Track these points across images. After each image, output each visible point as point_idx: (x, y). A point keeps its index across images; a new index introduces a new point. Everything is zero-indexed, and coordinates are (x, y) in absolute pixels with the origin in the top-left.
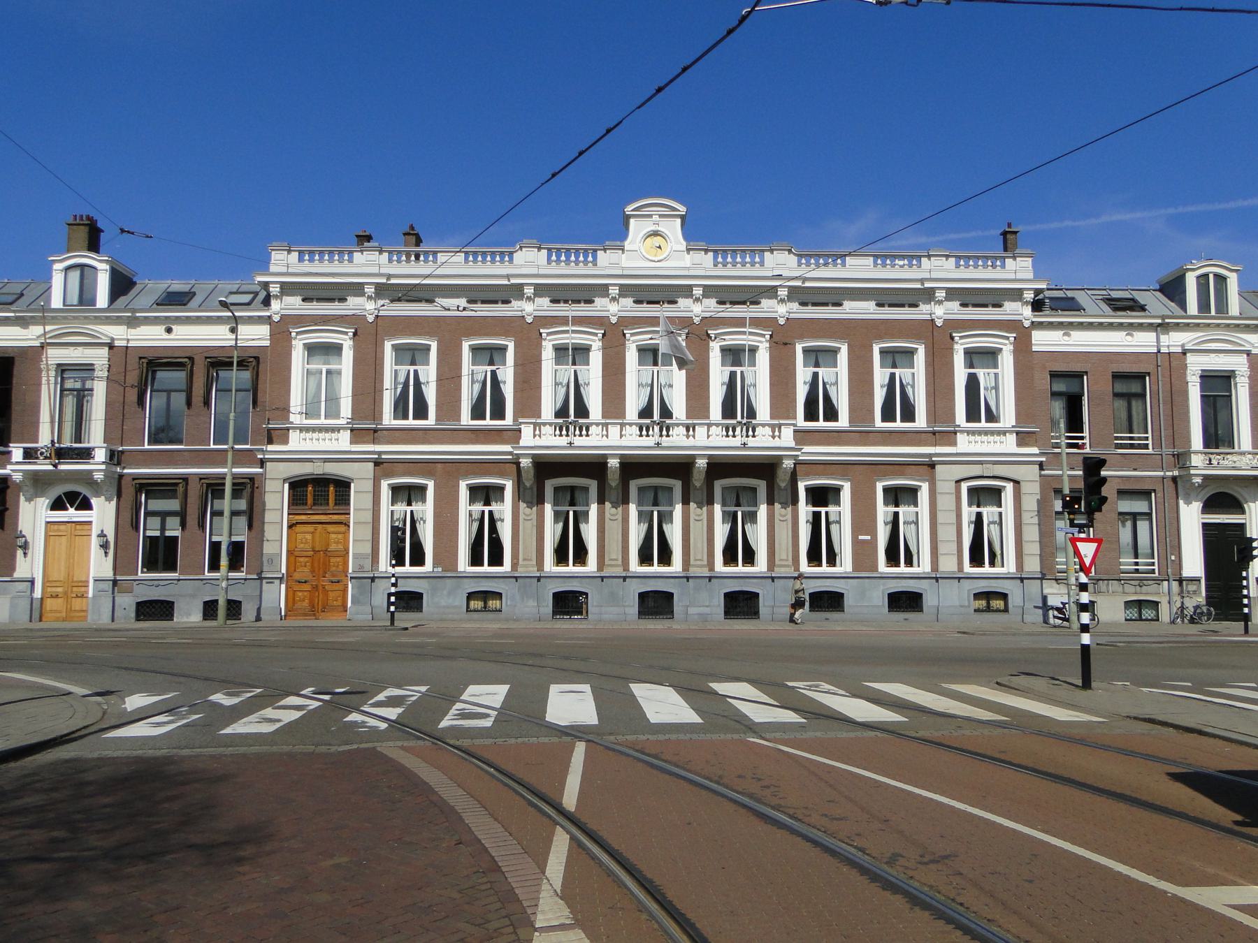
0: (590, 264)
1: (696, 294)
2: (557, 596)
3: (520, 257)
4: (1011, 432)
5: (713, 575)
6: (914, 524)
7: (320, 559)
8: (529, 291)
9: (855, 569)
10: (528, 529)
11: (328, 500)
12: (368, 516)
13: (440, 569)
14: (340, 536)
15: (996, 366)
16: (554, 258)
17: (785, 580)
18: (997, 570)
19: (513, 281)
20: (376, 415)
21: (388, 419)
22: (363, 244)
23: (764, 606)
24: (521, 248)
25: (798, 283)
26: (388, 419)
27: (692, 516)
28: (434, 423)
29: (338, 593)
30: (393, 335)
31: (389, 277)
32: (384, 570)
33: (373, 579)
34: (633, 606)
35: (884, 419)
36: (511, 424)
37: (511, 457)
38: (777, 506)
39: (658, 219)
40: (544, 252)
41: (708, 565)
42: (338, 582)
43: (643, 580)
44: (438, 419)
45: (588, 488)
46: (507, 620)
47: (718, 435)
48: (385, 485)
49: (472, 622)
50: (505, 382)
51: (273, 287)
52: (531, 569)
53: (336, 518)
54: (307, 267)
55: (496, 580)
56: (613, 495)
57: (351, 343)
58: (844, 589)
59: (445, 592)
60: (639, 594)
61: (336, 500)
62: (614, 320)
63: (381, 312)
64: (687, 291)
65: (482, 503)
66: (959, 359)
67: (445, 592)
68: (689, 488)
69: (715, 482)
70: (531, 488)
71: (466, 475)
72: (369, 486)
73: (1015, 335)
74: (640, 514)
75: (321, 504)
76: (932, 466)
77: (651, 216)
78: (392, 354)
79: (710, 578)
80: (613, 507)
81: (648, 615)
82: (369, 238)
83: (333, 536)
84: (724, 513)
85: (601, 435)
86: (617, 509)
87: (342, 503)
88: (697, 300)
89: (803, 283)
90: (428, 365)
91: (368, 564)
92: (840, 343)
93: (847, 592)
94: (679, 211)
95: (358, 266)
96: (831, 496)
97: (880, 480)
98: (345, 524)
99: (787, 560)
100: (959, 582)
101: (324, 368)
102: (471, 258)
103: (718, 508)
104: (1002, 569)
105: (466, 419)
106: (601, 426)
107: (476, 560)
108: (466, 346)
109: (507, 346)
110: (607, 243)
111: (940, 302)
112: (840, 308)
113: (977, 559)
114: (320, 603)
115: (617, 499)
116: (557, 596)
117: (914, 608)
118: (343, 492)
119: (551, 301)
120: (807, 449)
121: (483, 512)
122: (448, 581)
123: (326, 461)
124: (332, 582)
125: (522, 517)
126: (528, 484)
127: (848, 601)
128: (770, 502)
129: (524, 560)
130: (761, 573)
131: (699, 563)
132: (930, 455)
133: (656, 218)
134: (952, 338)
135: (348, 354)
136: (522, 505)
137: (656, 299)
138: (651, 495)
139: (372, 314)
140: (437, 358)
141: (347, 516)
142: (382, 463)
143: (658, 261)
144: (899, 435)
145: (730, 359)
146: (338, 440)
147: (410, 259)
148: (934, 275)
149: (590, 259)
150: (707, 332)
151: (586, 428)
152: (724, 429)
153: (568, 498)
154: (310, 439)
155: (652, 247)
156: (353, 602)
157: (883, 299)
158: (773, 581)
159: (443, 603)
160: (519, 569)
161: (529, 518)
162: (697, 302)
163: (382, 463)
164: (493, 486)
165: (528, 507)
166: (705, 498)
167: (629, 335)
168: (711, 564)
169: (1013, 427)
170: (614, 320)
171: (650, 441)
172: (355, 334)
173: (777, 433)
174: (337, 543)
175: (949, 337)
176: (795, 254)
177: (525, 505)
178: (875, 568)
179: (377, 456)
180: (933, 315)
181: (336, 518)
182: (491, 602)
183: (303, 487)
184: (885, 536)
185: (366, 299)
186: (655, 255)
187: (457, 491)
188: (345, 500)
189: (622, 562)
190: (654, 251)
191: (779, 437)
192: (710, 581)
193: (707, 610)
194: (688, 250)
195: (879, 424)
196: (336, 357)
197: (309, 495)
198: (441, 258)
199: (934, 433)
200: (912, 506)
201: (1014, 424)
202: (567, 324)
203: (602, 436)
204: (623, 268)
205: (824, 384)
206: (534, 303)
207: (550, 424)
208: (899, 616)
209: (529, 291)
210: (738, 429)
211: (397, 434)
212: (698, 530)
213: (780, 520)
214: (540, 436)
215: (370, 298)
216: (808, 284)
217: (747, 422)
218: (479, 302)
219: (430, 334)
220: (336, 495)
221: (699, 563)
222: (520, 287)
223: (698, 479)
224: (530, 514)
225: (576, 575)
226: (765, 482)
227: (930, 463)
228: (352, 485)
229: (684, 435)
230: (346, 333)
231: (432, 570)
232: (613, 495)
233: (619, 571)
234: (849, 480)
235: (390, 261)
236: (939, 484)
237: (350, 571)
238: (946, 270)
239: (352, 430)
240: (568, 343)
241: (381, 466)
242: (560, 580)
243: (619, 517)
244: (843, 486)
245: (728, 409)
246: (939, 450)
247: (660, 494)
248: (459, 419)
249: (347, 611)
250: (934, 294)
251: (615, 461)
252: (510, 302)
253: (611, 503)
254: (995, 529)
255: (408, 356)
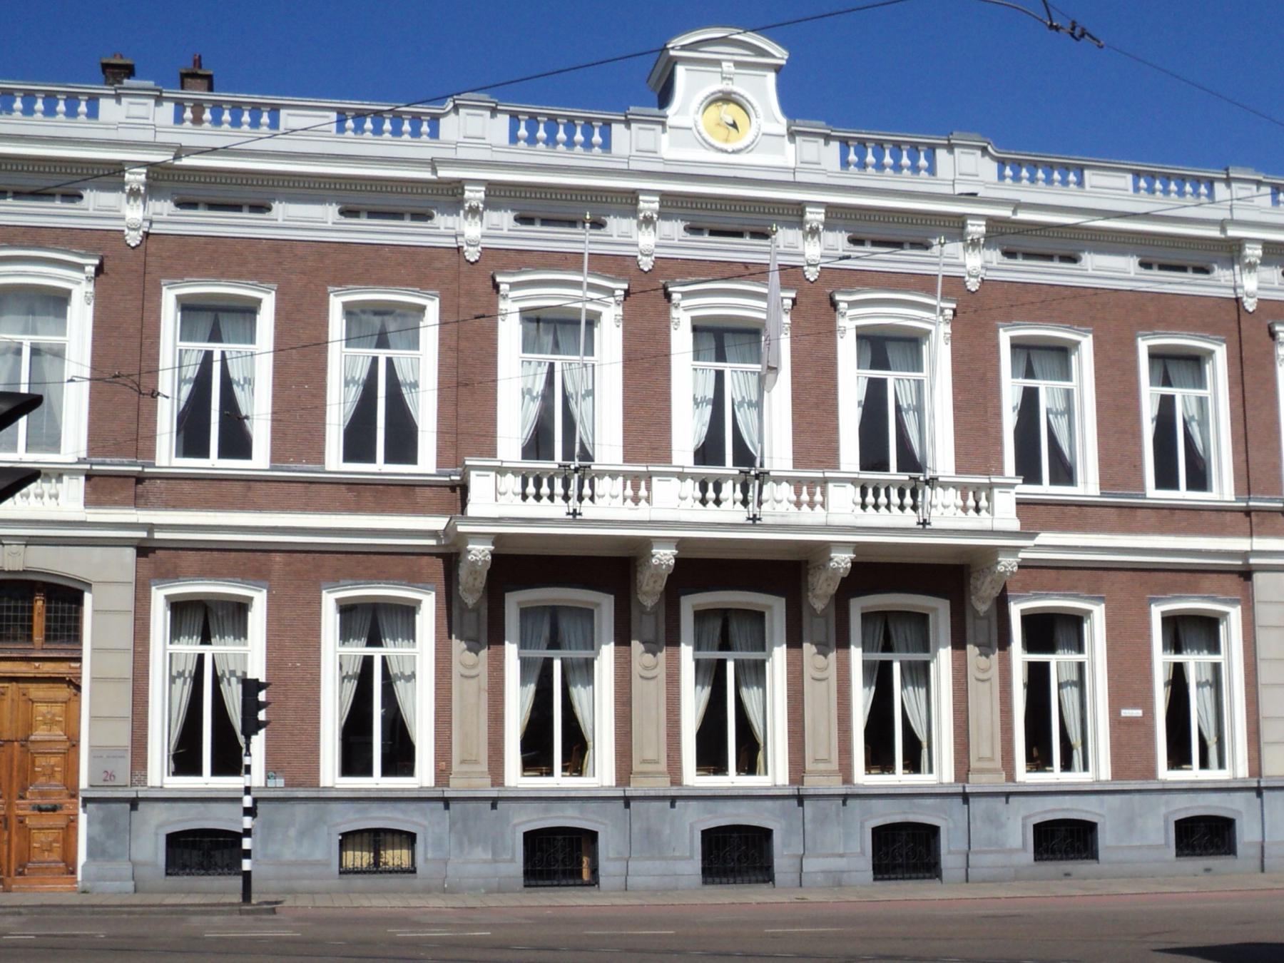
0: (597, 150)
1: (813, 220)
2: (535, 841)
3: (452, 126)
4: (73, 473)
5: (849, 792)
6: (1208, 687)
7: (12, 760)
8: (474, 195)
9: (1116, 774)
10: (469, 695)
11: (30, 628)
12: (125, 665)
13: (280, 782)
14: (57, 709)
15: (918, 367)
16: (523, 132)
17: (990, 799)
18: (1076, 777)
19: (444, 173)
20: (142, 442)
21: (166, 456)
22: (121, 83)
23: (950, 852)
24: (456, 108)
25: (1005, 212)
26: (166, 456)
27: (808, 672)
28: (267, 466)
29: (51, 836)
30: (179, 274)
31: (180, 151)
32: (158, 784)
33: (134, 803)
34: (691, 857)
35: (350, 455)
36: (433, 471)
37: (433, 542)
38: (972, 650)
39: (733, 69)
40: (504, 120)
41: (840, 770)
42: (54, 809)
43: (710, 804)
44: (277, 456)
45: (592, 611)
46: (428, 890)
47: (614, 497)
48: (159, 598)
49: (191, 895)
50: (415, 385)
51: (470, 191)
52: (477, 782)
53: (48, 668)
54: (352, 144)
55: (402, 805)
56: (647, 625)
57: (90, 288)
58: (1096, 814)
59: (292, 832)
60: (705, 833)
61: (48, 628)
62: (646, 263)
63: (154, 226)
64: (793, 214)
65: (364, 641)
66: (847, 348)
67: (292, 832)
68: (801, 613)
69: (507, 595)
70: (476, 609)
71: (336, 580)
72: (125, 598)
73: (954, 306)
74: (525, 664)
75: (15, 639)
76: (1246, 574)
77: (717, 63)
78: (176, 316)
79: (845, 798)
80: (647, 651)
81: (887, 872)
82: (129, 71)
83: (42, 708)
84: (698, 663)
85: (621, 498)
86: (655, 655)
87: (62, 637)
88: (648, 221)
89: (1014, 212)
90: (418, 349)
91: (123, 769)
92: (1079, 332)
93: (602, 826)
94: (773, 56)
95: (108, 126)
96: (1060, 634)
97: (1157, 601)
98: (70, 682)
99: (991, 759)
100: (1007, 802)
101: (27, 341)
102: (350, 124)
103: (511, 651)
104: (1222, 772)
105: (334, 460)
106: (620, 479)
107: (354, 761)
108: (336, 304)
109: (259, 301)
110: (632, 109)
111: (1251, 267)
112: (266, 215)
113: (879, 758)
114: (13, 856)
115: (827, 637)
116: (535, 841)
117: (1079, 851)
118: (63, 611)
119: (342, 213)
120: (1045, 538)
121: (201, 658)
122: (300, 809)
123: (30, 541)
124: (40, 810)
125: (457, 669)
126: (470, 600)
127: (1105, 839)
128: (794, 641)
129: (463, 762)
130: (602, 788)
131: (821, 766)
132: (1245, 555)
133: (728, 67)
134: (834, 305)
135: (429, 334)
136: (458, 646)
137: (1049, 252)
138: (715, 627)
139: (815, 265)
140: (276, 327)
141: (73, 665)
142: (153, 550)
143: (734, 152)
144: (1184, 514)
145: (709, 343)
146: (56, 497)
147: (11, 107)
148: (463, 154)
149: (597, 138)
150: (494, 280)
151: (874, 490)
152: (738, 487)
153: (546, 631)
154: (36, 496)
155: (719, 124)
156: (90, 854)
157: (354, 200)
158: (627, 805)
159: (288, 854)
160: (453, 782)
161: (473, 672)
162: (813, 238)
163: (153, 550)
164: (385, 605)
165: (470, 649)
166: (485, 627)
167: (507, 287)
168: (846, 771)
169: (80, 461)
170: (646, 263)
171: (545, 509)
172: (99, 270)
173: (643, 492)
174: (51, 723)
175: (1268, 334)
176: (993, 158)
177: (463, 645)
178: (1151, 772)
179: (144, 534)
180: (1239, 291)
181: (48, 668)
182: (390, 852)
183: (24, 598)
184: (697, 709)
185: (124, 196)
186: (727, 140)
187: (317, 614)
188: (69, 629)
189: (669, 765)
190: (722, 132)
191: (648, 500)
192: (494, 807)
193: (841, 863)
194: (792, 135)
195: (1154, 494)
196: (51, 319)
197: (36, 618)
198: (288, 119)
199: (1248, 512)
200: (1205, 652)
201: (83, 454)
202: (579, 270)
203: (625, 500)
204: (666, 161)
205: (898, 409)
206: (481, 220)
207: (515, 471)
208: (1195, 865)
209: (474, 195)
210: (727, 488)
211: (187, 487)
212: (819, 700)
213: (978, 680)
214: (592, 498)
215: (134, 194)
216: (1023, 216)
217: (581, 467)
218: (407, 216)
219: (259, 276)
220: (48, 619)
221: (821, 766)
222: (457, 187)
223: (649, 590)
224: (474, 666)
225: (573, 794)
226: (784, 600)
227: (1243, 569)
228: (88, 598)
229: (515, 494)
230: (80, 268)
231: (263, 785)
232: (647, 625)
233: (662, 786)
234: (1101, 599)
235: (179, 119)
236: (1259, 609)
237: (83, 783)
238: (1259, 208)
239: (89, 476)
240: (580, 309)
241: (151, 555)
242: (536, 805)
243: (661, 672)
244: (419, 602)
245: (873, 457)
246: (1260, 544)
247: (734, 628)
248: (321, 460)
249: (73, 872)
250: (463, 193)
251: (668, 552)
252: (430, 217)
253: (643, 642)
254: (1071, 695)
255: (205, 323)
